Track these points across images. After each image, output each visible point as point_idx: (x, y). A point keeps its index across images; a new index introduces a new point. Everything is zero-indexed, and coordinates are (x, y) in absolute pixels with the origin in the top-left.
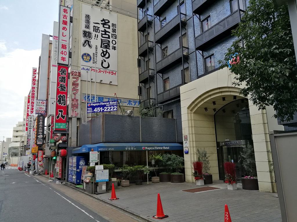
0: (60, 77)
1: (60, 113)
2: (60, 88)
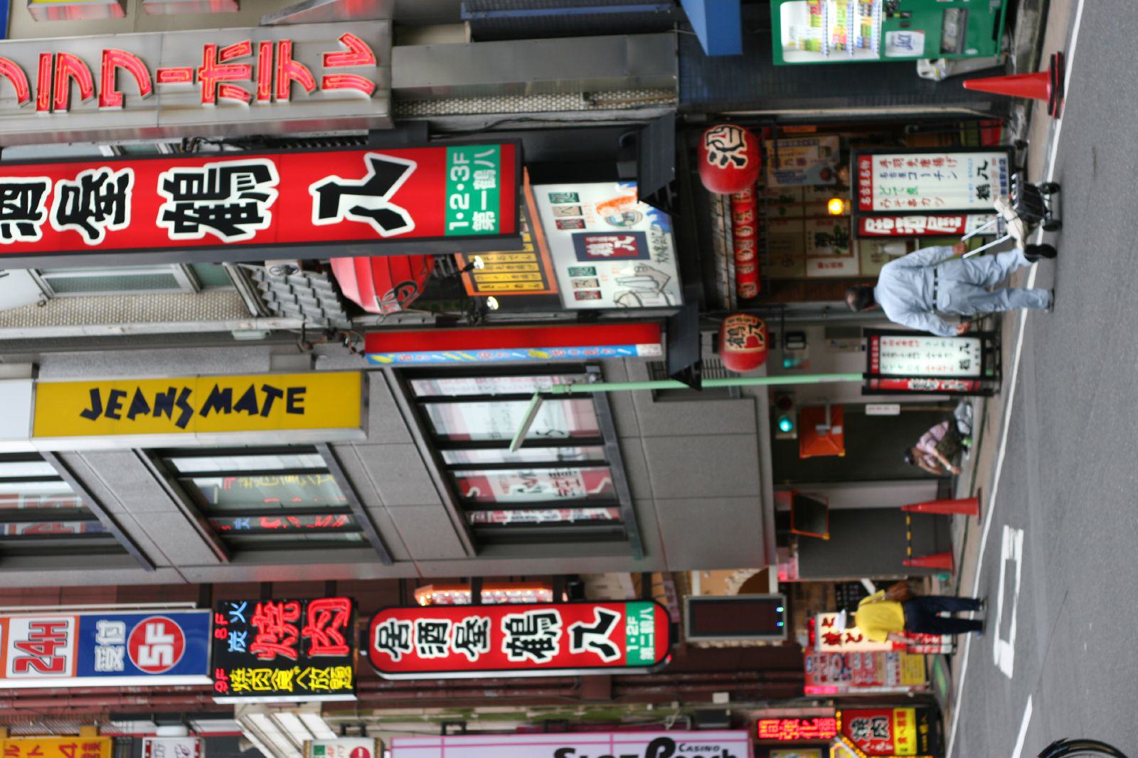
0: (423, 651)
1: (587, 638)
2: (99, 226)
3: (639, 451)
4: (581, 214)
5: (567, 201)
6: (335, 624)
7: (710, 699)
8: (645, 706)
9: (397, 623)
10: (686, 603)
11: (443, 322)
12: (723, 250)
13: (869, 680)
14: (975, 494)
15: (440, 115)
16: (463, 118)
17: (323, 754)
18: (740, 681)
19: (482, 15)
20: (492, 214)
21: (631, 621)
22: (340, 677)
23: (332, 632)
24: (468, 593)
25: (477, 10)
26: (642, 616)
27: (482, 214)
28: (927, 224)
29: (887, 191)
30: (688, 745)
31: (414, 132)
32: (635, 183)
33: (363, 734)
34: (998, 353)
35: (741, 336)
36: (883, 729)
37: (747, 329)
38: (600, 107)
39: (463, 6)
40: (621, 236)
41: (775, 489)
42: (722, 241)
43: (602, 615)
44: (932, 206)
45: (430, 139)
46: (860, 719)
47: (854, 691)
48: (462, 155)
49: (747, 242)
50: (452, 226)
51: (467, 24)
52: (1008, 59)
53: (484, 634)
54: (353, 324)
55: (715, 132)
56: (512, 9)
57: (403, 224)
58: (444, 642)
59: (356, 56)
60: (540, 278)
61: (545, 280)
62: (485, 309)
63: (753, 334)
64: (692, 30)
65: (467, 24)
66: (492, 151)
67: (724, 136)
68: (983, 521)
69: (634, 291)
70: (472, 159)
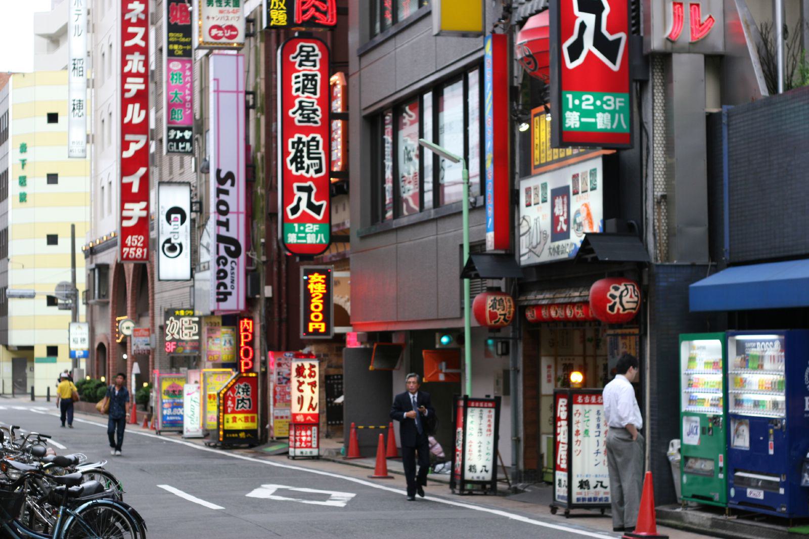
0: (297, 77)
1: (304, 196)
3: (428, 234)
4: (583, 192)
5: (591, 181)
6: (317, 14)
7: (267, 284)
8: (263, 238)
9: (318, 59)
10: (328, 267)
11: (514, 92)
12: (558, 295)
13: (278, 397)
14: (390, 474)
15: (653, 89)
16: (651, 107)
17: (234, 6)
18: (280, 306)
19: (725, 120)
20: (577, 125)
21: (316, 227)
22: (280, 17)
23: (312, 12)
24: (340, 110)
25: (728, 117)
26: (319, 235)
27: (578, 118)
28: (563, 443)
29: (587, 415)
30: (235, 267)
31: (641, 70)
32: (602, 231)
33: (248, 35)
34: (483, 493)
35: (499, 308)
36: (243, 406)
37: (503, 312)
38: (656, 207)
39: (732, 107)
40: (567, 222)
41: (406, 331)
42: (563, 295)
43: (321, 206)
44: (575, 447)
45: (636, 81)
46: (250, 390)
47: (271, 386)
48: (622, 104)
49: (563, 314)
50: (569, 96)
51: (720, 110)
52: (679, 505)
53: (309, 121)
54: (515, 25)
55: (634, 290)
56: (729, 143)
57: (572, 60)
58: (303, 93)
59: (697, 27)
60: (542, 162)
61: (541, 165)
62: (520, 122)
63: (499, 317)
64: (710, 274)
65: (720, 110)
66: (625, 127)
67: (631, 297)
68: (370, 479)
69: (531, 230)
70: (619, 112)
